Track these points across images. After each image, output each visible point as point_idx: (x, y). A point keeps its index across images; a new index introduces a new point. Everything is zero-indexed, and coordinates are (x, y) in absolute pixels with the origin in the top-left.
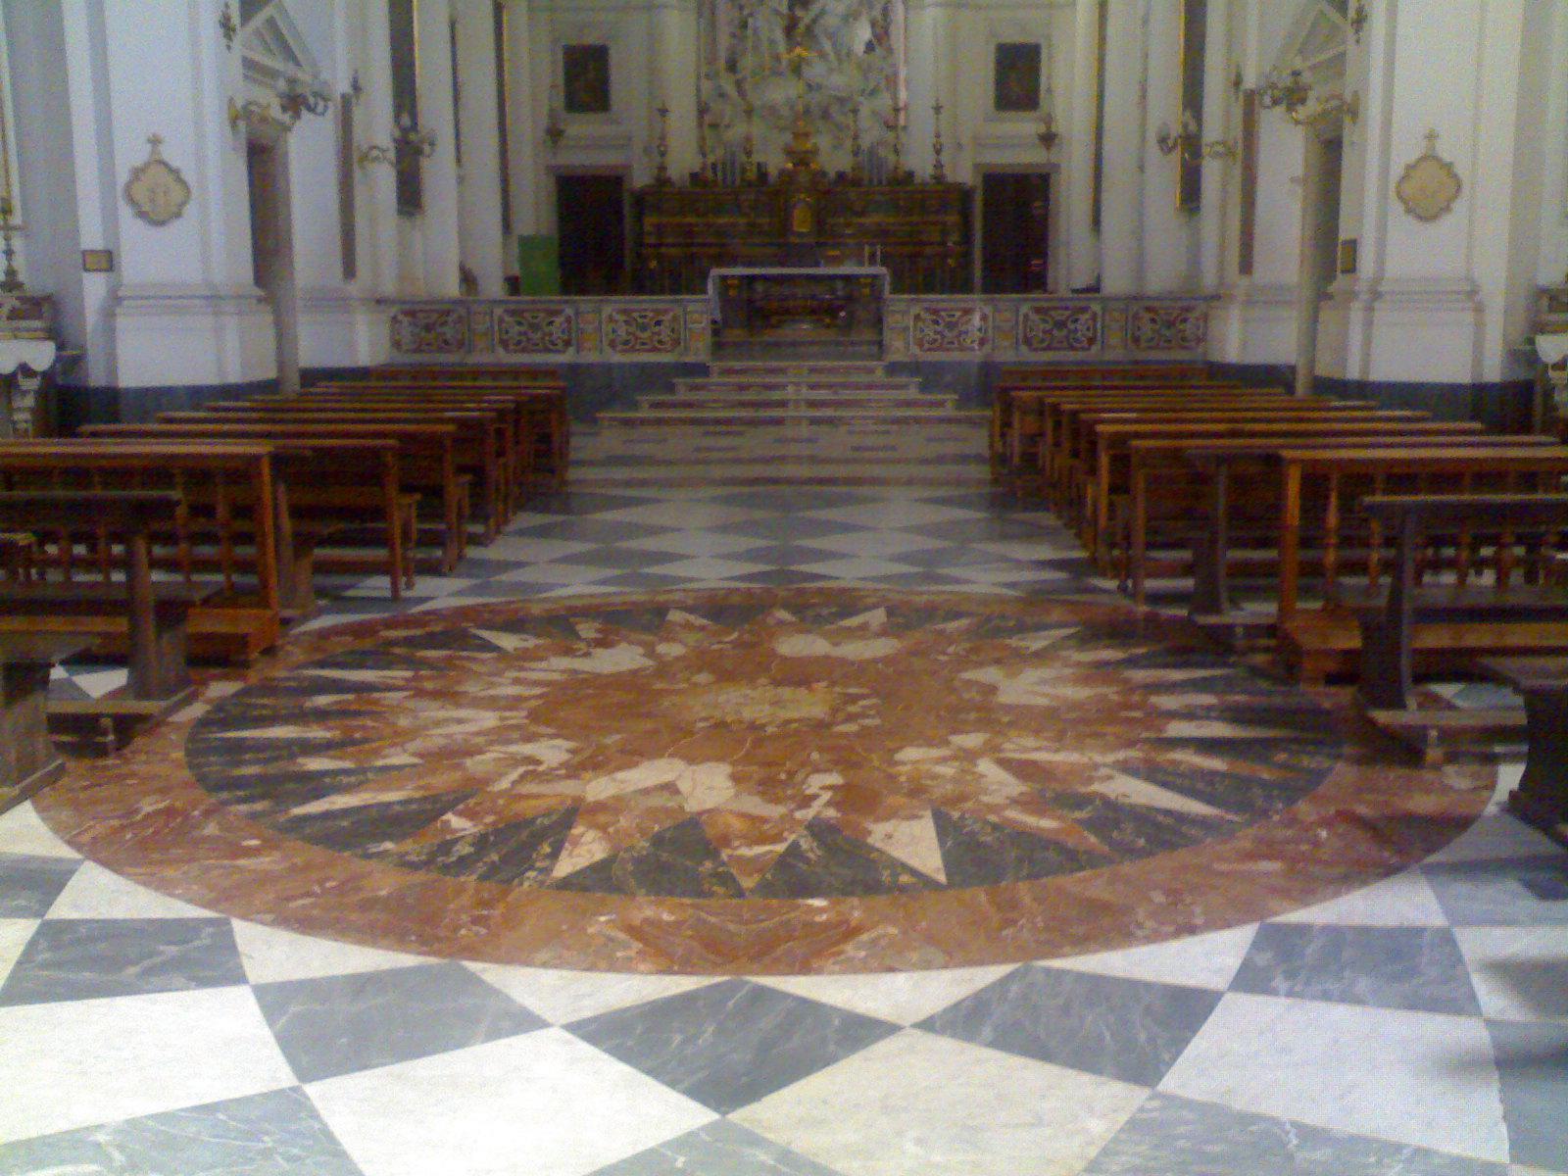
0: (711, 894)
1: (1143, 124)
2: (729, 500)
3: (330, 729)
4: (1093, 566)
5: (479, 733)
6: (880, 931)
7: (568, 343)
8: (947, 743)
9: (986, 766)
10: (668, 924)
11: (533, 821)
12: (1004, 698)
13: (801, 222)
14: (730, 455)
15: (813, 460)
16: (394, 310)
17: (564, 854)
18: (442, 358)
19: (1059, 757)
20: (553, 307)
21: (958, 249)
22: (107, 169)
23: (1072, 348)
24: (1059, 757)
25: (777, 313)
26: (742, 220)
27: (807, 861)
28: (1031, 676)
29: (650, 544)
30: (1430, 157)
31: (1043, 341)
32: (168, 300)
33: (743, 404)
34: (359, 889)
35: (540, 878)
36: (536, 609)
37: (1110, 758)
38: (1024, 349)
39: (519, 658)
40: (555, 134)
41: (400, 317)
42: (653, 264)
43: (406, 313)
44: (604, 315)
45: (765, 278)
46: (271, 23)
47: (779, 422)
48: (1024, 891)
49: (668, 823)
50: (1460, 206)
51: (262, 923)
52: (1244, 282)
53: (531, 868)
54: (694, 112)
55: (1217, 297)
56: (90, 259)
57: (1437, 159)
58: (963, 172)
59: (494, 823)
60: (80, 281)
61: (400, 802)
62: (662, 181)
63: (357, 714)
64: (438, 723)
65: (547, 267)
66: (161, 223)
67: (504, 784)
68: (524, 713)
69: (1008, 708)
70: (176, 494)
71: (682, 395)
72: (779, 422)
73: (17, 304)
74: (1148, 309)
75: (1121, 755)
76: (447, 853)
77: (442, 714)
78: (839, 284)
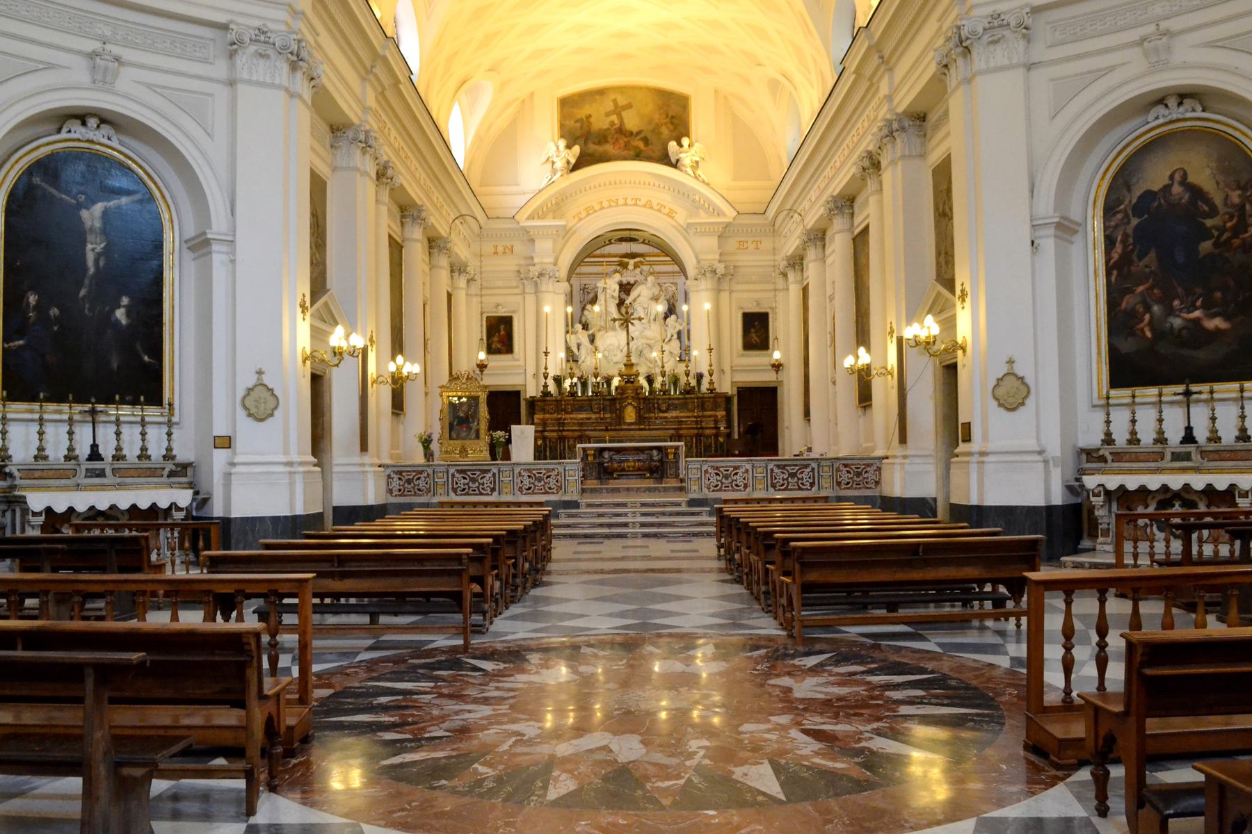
0: (646, 809)
1: (1037, 401)
2: (601, 583)
3: (392, 716)
5: (481, 719)
6: (752, 827)
7: (493, 490)
8: (769, 721)
9: (794, 733)
10: (623, 825)
11: (528, 767)
12: (798, 694)
13: (630, 415)
15: (644, 558)
16: (389, 471)
17: (551, 787)
19: (839, 727)
20: (486, 468)
23: (800, 489)
24: (839, 727)
25: (617, 471)
26: (593, 416)
27: (700, 789)
28: (810, 681)
31: (783, 485)
33: (601, 525)
34: (433, 806)
35: (540, 800)
37: (869, 727)
38: (771, 490)
39: (495, 675)
41: (392, 475)
43: (396, 473)
45: (610, 449)
48: (833, 804)
49: (609, 769)
50: (1030, 402)
51: (379, 826)
53: (533, 794)
56: (218, 441)
58: (726, 387)
59: (504, 769)
60: (211, 455)
61: (444, 758)
63: (406, 707)
64: (457, 713)
66: (262, 420)
67: (505, 747)
68: (507, 707)
69: (803, 700)
73: (174, 468)
74: (846, 466)
75: (875, 725)
76: (481, 786)
77: (457, 708)
78: (655, 452)
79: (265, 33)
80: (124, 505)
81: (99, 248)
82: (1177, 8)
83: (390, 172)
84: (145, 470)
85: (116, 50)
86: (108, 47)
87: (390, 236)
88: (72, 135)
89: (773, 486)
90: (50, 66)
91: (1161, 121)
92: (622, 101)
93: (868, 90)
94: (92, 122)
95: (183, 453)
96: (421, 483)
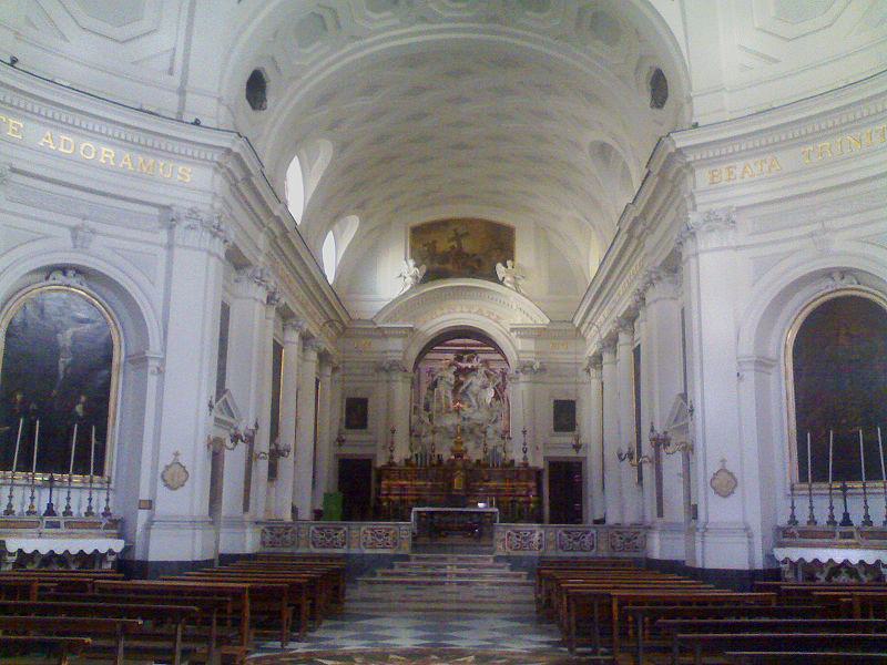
4: (558, 644)
13: (458, 483)
14: (419, 599)
16: (262, 527)
18: (329, 551)
21: (536, 499)
22: (154, 467)
29: (381, 633)
30: (723, 470)
32: (176, 523)
36: (338, 653)
38: (560, 551)
40: (341, 441)
42: (385, 504)
44: (363, 529)
46: (225, 402)
47: (442, 583)
50: (738, 491)
52: (660, 520)
54: (408, 432)
55: (650, 528)
57: (726, 471)
62: (391, 464)
65: (336, 508)
66: (175, 489)
70: (229, 599)
71: (397, 570)
72: (442, 583)
74: (619, 533)
79: (195, 213)
80: (74, 551)
81: (68, 360)
82: (835, 213)
83: (277, 297)
84: (87, 524)
85: (91, 224)
86: (88, 223)
87: (274, 341)
88: (56, 282)
89: (562, 548)
90: (47, 237)
91: (830, 289)
92: (461, 230)
93: (637, 246)
94: (71, 273)
95: (117, 513)
96: (288, 537)
